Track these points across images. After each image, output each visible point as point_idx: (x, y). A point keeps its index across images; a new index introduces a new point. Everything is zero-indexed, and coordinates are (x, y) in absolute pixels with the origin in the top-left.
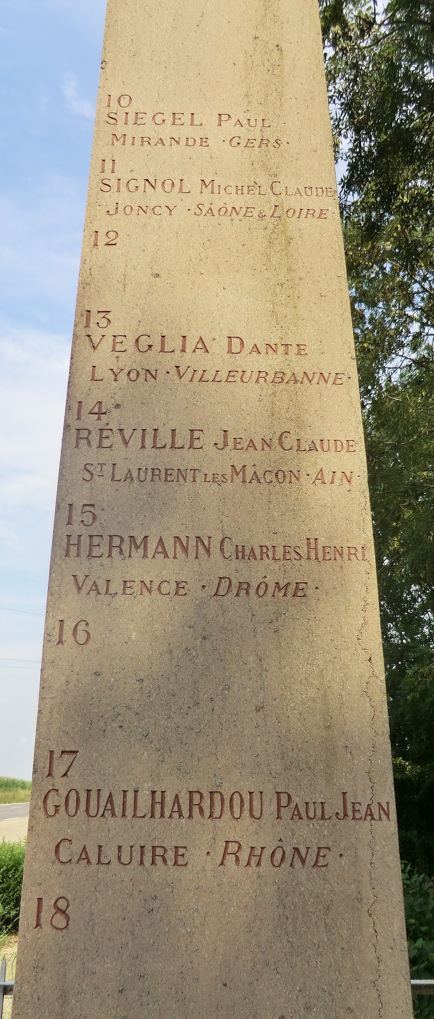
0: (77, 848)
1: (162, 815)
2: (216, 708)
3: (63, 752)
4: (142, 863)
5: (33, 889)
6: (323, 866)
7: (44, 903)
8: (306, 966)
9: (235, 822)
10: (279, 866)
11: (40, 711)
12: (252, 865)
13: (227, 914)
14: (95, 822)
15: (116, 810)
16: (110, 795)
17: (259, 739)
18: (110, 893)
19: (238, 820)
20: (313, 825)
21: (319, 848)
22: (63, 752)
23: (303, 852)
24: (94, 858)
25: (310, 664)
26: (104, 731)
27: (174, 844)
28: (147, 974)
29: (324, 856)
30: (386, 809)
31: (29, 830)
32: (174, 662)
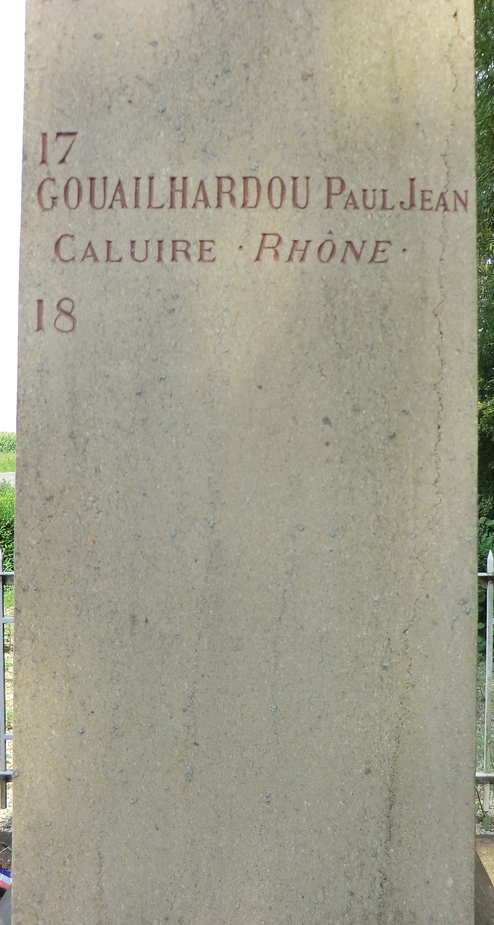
0: (81, 245)
1: (184, 205)
2: (252, 76)
3: (59, 134)
4: (160, 259)
5: (30, 290)
6: (381, 262)
7: (45, 305)
8: (357, 368)
9: (274, 211)
10: (328, 261)
11: (27, 86)
12: (294, 260)
13: (263, 314)
14: (101, 214)
15: (127, 199)
16: (119, 184)
17: (306, 114)
18: (123, 293)
19: (278, 210)
20: (372, 215)
21: (378, 242)
22: (59, 134)
23: (358, 245)
24: (102, 255)
25: (375, 21)
26: (109, 107)
27: (198, 237)
28: (169, 376)
29: (383, 251)
30: (463, 198)
31: (22, 226)
32: (198, 20)
